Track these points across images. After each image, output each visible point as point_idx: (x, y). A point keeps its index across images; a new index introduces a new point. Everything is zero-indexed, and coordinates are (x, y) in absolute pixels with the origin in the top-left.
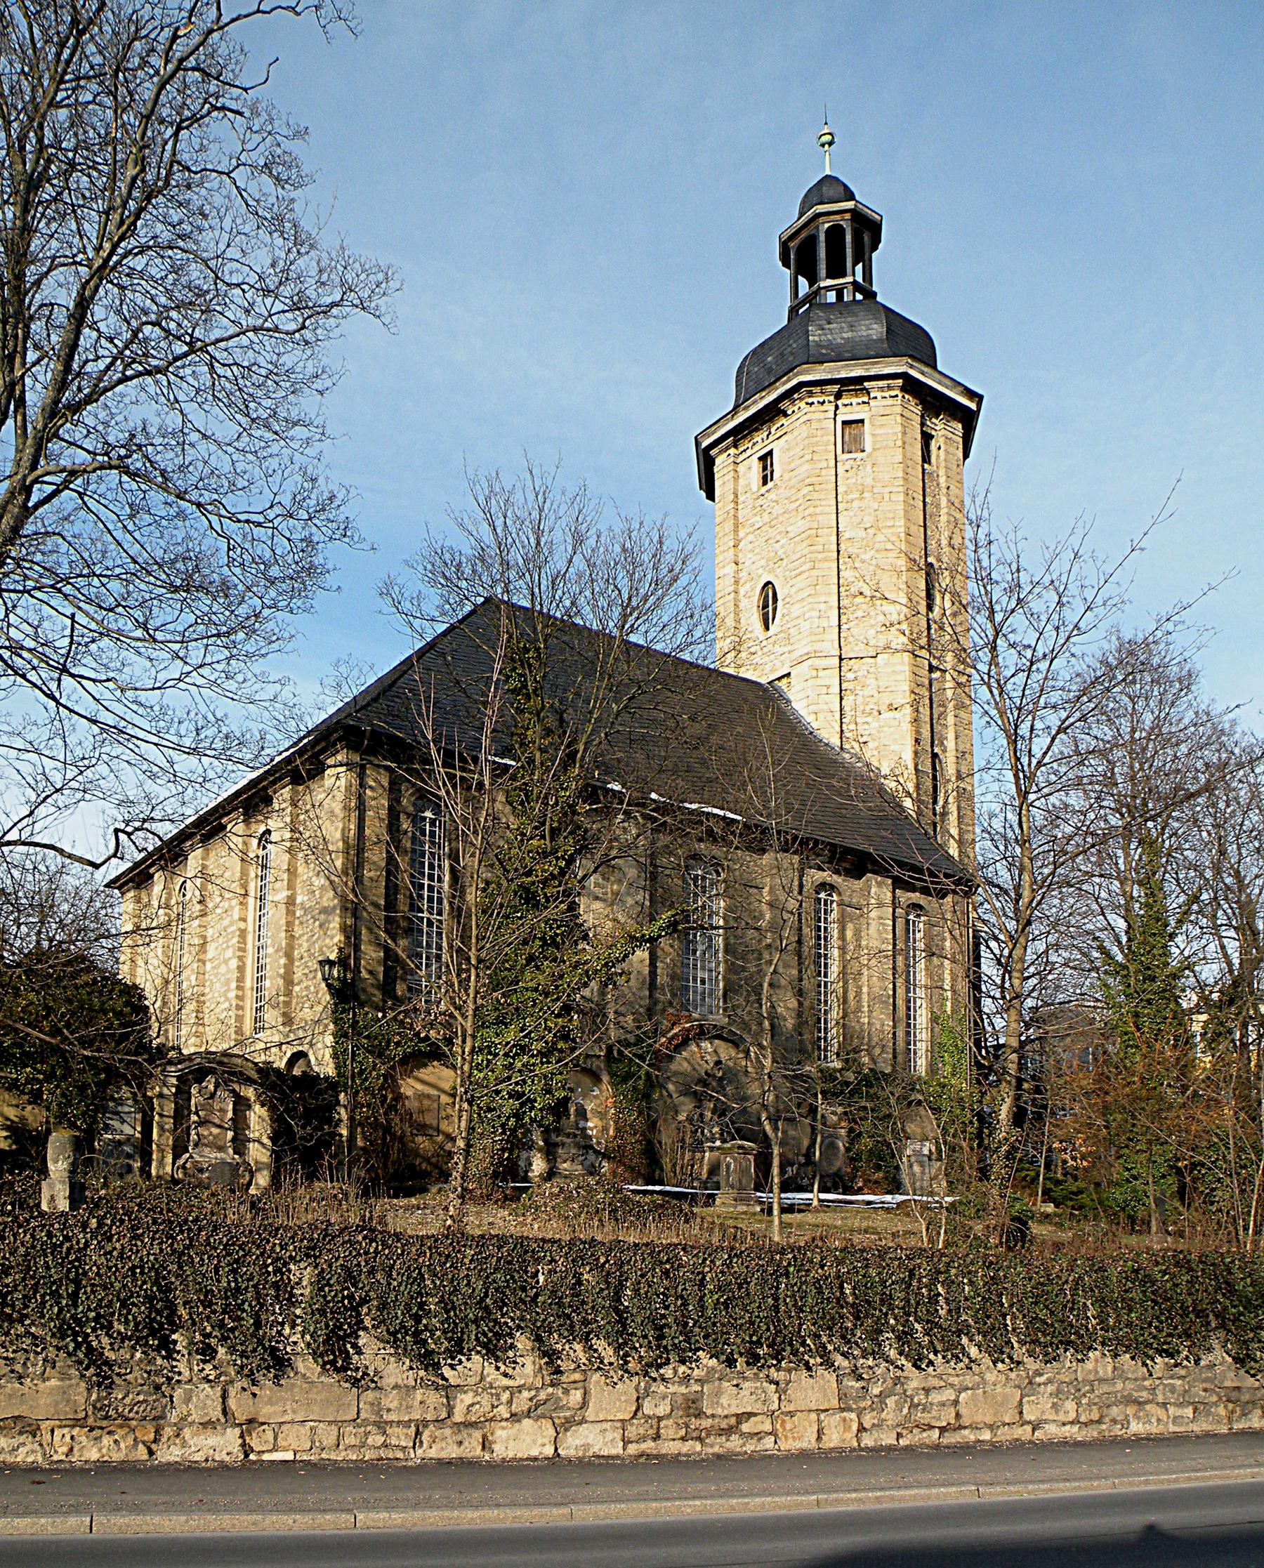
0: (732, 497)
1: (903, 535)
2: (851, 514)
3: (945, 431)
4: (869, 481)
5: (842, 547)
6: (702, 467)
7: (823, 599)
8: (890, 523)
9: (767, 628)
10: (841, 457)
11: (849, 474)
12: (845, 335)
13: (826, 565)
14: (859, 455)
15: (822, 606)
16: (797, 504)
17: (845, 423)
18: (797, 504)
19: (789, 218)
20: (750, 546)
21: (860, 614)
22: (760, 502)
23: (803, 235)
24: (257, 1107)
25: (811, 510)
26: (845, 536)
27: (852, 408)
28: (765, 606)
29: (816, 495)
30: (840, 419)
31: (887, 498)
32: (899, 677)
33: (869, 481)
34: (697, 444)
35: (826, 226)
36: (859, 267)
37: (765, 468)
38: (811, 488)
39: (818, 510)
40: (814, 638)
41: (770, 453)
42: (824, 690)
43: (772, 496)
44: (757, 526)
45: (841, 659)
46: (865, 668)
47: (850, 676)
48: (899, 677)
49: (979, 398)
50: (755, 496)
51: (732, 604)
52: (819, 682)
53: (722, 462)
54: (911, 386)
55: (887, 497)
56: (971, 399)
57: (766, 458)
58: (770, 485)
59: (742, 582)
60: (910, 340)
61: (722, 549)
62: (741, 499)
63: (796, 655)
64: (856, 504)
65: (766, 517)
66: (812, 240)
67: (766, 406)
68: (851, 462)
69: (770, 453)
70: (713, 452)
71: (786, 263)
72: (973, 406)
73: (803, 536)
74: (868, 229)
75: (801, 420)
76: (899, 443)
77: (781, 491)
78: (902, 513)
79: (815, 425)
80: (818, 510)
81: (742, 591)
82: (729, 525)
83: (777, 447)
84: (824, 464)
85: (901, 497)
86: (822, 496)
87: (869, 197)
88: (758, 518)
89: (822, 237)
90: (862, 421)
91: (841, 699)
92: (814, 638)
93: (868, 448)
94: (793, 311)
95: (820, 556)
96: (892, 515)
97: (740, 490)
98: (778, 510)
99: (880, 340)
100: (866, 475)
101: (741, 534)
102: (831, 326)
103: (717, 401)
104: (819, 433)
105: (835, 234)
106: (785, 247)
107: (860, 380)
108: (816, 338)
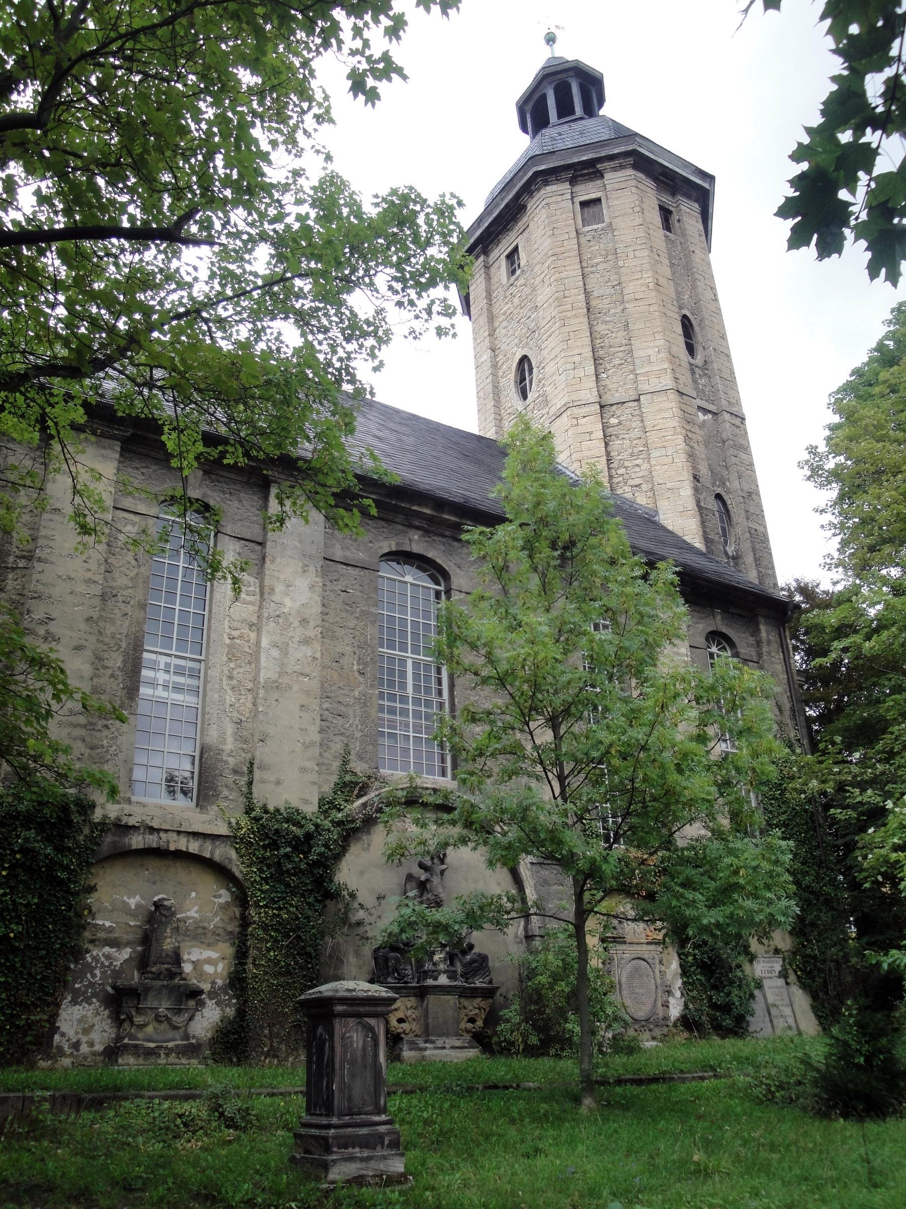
3: (687, 211)
7: (576, 351)
9: (525, 397)
11: (591, 243)
13: (578, 320)
15: (577, 359)
20: (504, 331)
22: (513, 290)
24: (608, 872)
25: (557, 275)
27: (587, 191)
28: (523, 379)
32: (666, 415)
38: (555, 258)
40: (570, 389)
42: (587, 437)
45: (602, 407)
46: (627, 411)
47: (614, 421)
48: (666, 415)
49: (711, 178)
52: (580, 429)
55: (631, 255)
58: (518, 272)
63: (553, 410)
67: (507, 206)
69: (516, 249)
72: (706, 185)
79: (553, 207)
80: (563, 275)
83: (521, 242)
85: (646, 253)
88: (510, 305)
90: (598, 201)
91: (607, 444)
92: (570, 389)
95: (569, 314)
96: (638, 269)
101: (496, 324)
107: (592, 163)
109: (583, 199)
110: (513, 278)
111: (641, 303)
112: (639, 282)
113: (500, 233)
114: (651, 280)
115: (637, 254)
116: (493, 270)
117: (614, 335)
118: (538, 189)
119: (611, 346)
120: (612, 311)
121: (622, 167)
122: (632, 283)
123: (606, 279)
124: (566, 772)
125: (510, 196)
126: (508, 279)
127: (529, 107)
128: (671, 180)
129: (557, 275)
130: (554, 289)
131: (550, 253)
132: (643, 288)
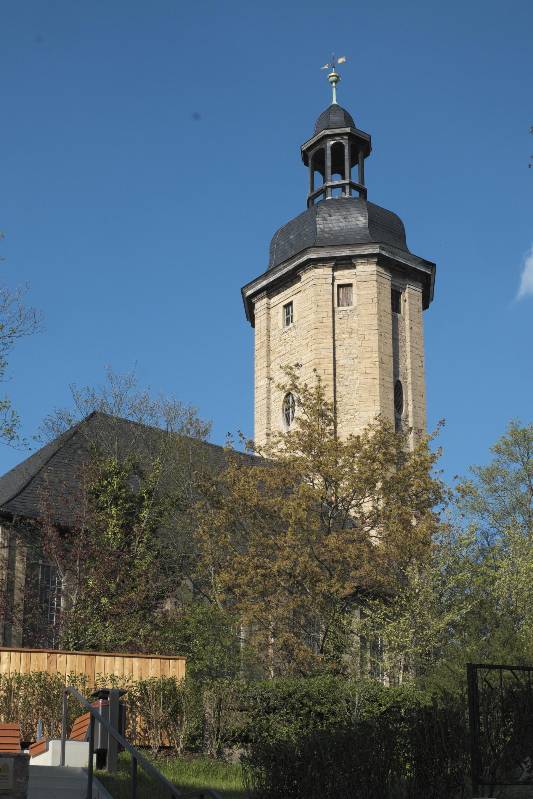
0: (266, 332)
1: (377, 363)
2: (343, 348)
4: (355, 325)
5: (338, 370)
6: (246, 304)
8: (369, 355)
10: (338, 309)
12: (341, 224)
14: (349, 308)
16: (307, 341)
17: (340, 286)
18: (307, 341)
19: (308, 139)
21: (349, 417)
22: (285, 336)
23: (318, 148)
26: (339, 363)
27: (343, 276)
29: (319, 336)
30: (337, 283)
31: (367, 339)
33: (355, 325)
34: (243, 294)
35: (332, 143)
36: (356, 168)
37: (288, 314)
38: (316, 331)
39: (321, 345)
41: (291, 304)
43: (292, 333)
44: (282, 353)
49: (432, 266)
50: (281, 332)
51: (265, 406)
53: (260, 305)
54: (382, 261)
55: (367, 337)
56: (428, 268)
57: (288, 306)
58: (291, 325)
59: (272, 391)
60: (386, 228)
61: (259, 368)
62: (272, 333)
64: (347, 342)
65: (288, 348)
66: (322, 152)
68: (343, 313)
69: (291, 304)
70: (254, 300)
71: (306, 164)
73: (311, 363)
74: (361, 146)
75: (310, 284)
76: (375, 300)
77: (297, 330)
78: (377, 348)
80: (321, 345)
81: (272, 398)
82: (263, 352)
83: (296, 300)
84: (325, 315)
85: (376, 337)
86: (323, 337)
87: (362, 125)
89: (329, 151)
90: (350, 285)
93: (355, 304)
94: (311, 199)
96: (370, 350)
97: (272, 327)
98: (295, 343)
99: (364, 228)
100: (354, 322)
102: (332, 218)
103: (256, 262)
104: (322, 293)
105: (338, 149)
106: (305, 155)
107: (350, 258)
108: (322, 226)
109: (340, 282)
110: (287, 328)
111: (369, 376)
112: (370, 360)
113: (281, 287)
114: (377, 359)
115: (371, 337)
116: (272, 312)
117: (349, 396)
118: (311, 269)
119: (346, 404)
120: (350, 378)
121: (369, 263)
122: (364, 361)
123: (348, 352)
124: (514, 671)
125: (290, 267)
126: (284, 327)
127: (311, 154)
128: (404, 269)
129: (316, 345)
130: (314, 356)
131: (314, 326)
132: (372, 365)
